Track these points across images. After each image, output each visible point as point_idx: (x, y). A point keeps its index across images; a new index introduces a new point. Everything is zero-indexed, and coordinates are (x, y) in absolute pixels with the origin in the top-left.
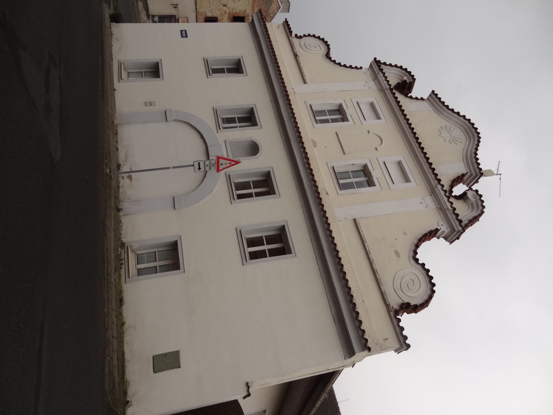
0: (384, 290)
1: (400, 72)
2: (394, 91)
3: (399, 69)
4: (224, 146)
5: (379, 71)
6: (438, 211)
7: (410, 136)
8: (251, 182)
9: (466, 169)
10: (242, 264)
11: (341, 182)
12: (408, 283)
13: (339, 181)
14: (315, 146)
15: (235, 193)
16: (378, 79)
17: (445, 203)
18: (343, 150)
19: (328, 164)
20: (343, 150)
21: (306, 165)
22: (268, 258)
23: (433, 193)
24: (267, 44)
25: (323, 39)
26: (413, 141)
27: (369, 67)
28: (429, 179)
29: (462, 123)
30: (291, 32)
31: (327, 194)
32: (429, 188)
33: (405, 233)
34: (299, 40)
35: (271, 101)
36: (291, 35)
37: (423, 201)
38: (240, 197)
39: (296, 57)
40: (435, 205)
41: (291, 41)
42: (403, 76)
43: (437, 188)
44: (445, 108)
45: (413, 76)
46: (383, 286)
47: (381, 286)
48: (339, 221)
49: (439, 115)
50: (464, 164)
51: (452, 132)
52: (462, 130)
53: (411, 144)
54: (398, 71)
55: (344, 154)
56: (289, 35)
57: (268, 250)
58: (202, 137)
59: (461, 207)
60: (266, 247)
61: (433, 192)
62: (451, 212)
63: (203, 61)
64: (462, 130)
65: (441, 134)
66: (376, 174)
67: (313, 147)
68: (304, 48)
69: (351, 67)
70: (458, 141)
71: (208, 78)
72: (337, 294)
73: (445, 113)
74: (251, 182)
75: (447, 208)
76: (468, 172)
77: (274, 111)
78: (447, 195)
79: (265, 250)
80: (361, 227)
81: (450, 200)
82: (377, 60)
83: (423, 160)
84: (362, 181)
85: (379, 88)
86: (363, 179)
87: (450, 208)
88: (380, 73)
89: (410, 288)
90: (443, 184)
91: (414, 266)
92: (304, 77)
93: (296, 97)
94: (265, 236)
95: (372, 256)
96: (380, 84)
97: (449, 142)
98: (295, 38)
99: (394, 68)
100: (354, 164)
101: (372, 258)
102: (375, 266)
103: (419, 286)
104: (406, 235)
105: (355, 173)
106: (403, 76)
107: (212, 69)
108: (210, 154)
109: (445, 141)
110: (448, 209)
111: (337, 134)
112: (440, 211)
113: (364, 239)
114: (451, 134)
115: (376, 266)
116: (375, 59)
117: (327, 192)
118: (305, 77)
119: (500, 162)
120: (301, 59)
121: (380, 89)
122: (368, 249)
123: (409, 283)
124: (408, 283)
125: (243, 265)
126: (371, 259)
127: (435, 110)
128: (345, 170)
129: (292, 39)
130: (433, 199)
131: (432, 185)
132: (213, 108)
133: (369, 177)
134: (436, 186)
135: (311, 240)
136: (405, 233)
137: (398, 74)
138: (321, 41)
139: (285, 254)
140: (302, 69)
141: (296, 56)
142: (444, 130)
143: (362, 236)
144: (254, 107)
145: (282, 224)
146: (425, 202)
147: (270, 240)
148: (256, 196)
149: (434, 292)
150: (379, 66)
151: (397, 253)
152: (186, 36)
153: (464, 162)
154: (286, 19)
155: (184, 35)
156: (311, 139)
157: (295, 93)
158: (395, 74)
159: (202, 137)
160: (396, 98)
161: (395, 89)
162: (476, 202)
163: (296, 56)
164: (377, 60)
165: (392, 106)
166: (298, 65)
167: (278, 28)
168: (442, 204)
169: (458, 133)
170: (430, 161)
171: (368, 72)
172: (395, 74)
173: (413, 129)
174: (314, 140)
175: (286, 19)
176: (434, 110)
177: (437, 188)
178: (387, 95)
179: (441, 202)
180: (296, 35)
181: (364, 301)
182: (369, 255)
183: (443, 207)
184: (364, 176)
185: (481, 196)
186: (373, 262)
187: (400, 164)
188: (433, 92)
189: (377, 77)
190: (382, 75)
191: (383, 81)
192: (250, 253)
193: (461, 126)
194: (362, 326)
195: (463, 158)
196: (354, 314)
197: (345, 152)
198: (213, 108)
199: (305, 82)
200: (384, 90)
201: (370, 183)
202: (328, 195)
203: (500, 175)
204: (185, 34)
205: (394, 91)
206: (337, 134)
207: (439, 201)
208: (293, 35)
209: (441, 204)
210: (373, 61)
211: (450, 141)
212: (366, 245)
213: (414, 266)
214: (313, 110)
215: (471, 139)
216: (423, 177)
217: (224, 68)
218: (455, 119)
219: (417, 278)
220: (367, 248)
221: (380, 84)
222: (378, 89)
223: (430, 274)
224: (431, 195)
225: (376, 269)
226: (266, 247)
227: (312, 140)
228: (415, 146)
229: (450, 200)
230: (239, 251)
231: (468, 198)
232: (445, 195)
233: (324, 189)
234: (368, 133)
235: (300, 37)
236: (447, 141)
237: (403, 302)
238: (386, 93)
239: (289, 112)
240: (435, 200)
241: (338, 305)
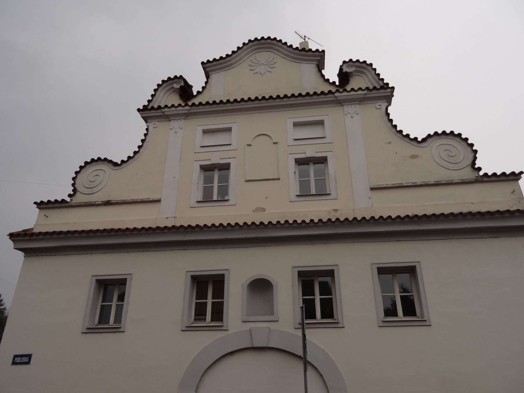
0: (459, 180)
1: (163, 89)
2: (190, 103)
3: (160, 89)
4: (252, 325)
5: (159, 111)
6: (363, 104)
7: (264, 104)
8: (304, 297)
9: (311, 64)
10: (429, 327)
11: (299, 193)
12: (449, 155)
13: (225, 199)
14: (264, 210)
15: (320, 320)
16: (172, 115)
17: (357, 95)
18: (273, 179)
19: (292, 200)
20: (273, 179)
21: (396, 221)
22: (225, 300)
23: (169, 118)
24: (98, 236)
25: (93, 160)
26: (271, 103)
27: (146, 122)
28: (270, 106)
29: (250, 49)
30: (63, 201)
31: (335, 211)
32: (333, 105)
33: (389, 143)
34: (78, 194)
35: (148, 251)
36: (67, 202)
37: (174, 130)
38: (118, 319)
39: (109, 203)
40: (348, 106)
41: (79, 204)
42: (171, 86)
43: (337, 97)
44: (228, 59)
45: (176, 77)
46: (455, 180)
47: (454, 181)
48: (372, 206)
49: (233, 68)
50: (303, 63)
51: (259, 62)
52: (258, 52)
53: (273, 106)
54: (162, 91)
55: (279, 179)
56: (67, 205)
57: (213, 298)
58: (231, 353)
59: (355, 83)
60: (210, 301)
61: (340, 103)
62: (368, 92)
63: (187, 333)
64: (258, 52)
65: (261, 73)
66: (216, 158)
67: (265, 212)
68: (95, 190)
69: (143, 141)
70: (272, 60)
71: (124, 332)
72: (319, 234)
73: (232, 62)
74: (304, 297)
75: (363, 95)
76: (316, 63)
77: (337, 243)
78: (184, 105)
79: (212, 302)
80: (383, 185)
81: (349, 89)
82: (141, 108)
83: (298, 100)
84: (204, 177)
85: (184, 117)
86: (216, 175)
87: (365, 92)
88: (163, 110)
89: (454, 155)
90: (177, 105)
91: (429, 144)
92: (416, 184)
93: (182, 217)
94: (196, 299)
95: (419, 182)
96: (179, 115)
97: (272, 68)
98: (73, 198)
99: (158, 93)
100: (295, 172)
101: (422, 182)
102: (430, 182)
103: (452, 146)
104: (391, 142)
105: (208, 180)
106: (171, 86)
107: (100, 322)
108: (265, 346)
109: (271, 72)
110: (365, 94)
111: (247, 181)
112: (362, 103)
113: (397, 185)
114: (262, 64)
115: (432, 181)
116: (139, 110)
117: (334, 210)
118: (149, 198)
119: (296, 32)
120: (114, 197)
121: (185, 117)
122: (411, 184)
123: (448, 154)
124: (449, 155)
125: (227, 330)
126: (422, 183)
127: (226, 69)
128: (201, 190)
129: (73, 202)
130: (348, 105)
131: (160, 116)
132: (182, 331)
133: (216, 168)
134: (336, 97)
135: (398, 241)
136: (389, 143)
137: (166, 92)
138: (88, 166)
139: (224, 281)
140: (135, 200)
141: (108, 203)
142: (255, 69)
143: (394, 186)
144: (96, 279)
145: (94, 282)
146: (176, 129)
147: (201, 294)
148: (123, 301)
149: (106, 159)
150: (153, 108)
151: (414, 157)
152: (29, 356)
153: (301, 63)
154: (35, 203)
155: (25, 359)
156: (252, 213)
157: (175, 217)
158: (164, 94)
159: (231, 353)
160: (200, 104)
161: (187, 102)
162: (356, 67)
163: (108, 203)
164: (141, 108)
165: (215, 111)
166: (127, 204)
167: (47, 217)
168: (357, 98)
169: (264, 56)
170: (218, 101)
171: (155, 124)
172: (164, 94)
173: (242, 100)
174: (254, 209)
175: (35, 203)
176: (225, 71)
177: (165, 113)
178: (198, 112)
179: (355, 99)
180: (70, 196)
181: (472, 202)
182: (418, 184)
183: (361, 98)
184: (213, 172)
185: (351, 60)
186: (427, 183)
187: (205, 132)
188: (203, 63)
189: (167, 115)
190: (166, 110)
191: (176, 110)
192: (213, 320)
193: (252, 51)
194: (265, 223)
195: (296, 62)
196: (158, 231)
197: (276, 177)
198: (182, 331)
199: (159, 201)
200: (189, 113)
201: (226, 167)
202: (337, 210)
203: (306, 38)
204: (23, 358)
205: (190, 103)
206: (247, 181)
207: (352, 100)
208: (68, 199)
209: (359, 98)
210: (140, 114)
211: (272, 67)
212: (406, 185)
213: (429, 144)
214: (202, 200)
215: (272, 47)
216: (262, 111)
217: (101, 305)
218: (244, 54)
219: (441, 146)
220: (409, 184)
221: (179, 115)
222: (184, 119)
223: (440, 132)
224: (170, 120)
225: (434, 181)
226: (210, 301)
227: (254, 211)
228: (278, 102)
229: (349, 89)
230: (411, 327)
231: (351, 73)
232: (341, 92)
233: (329, 212)
234: (251, 146)
235: (75, 190)
236: (271, 70)
237: (469, 165)
238: (194, 113)
239: (214, 230)
240: (350, 103)
241: (56, 248)
